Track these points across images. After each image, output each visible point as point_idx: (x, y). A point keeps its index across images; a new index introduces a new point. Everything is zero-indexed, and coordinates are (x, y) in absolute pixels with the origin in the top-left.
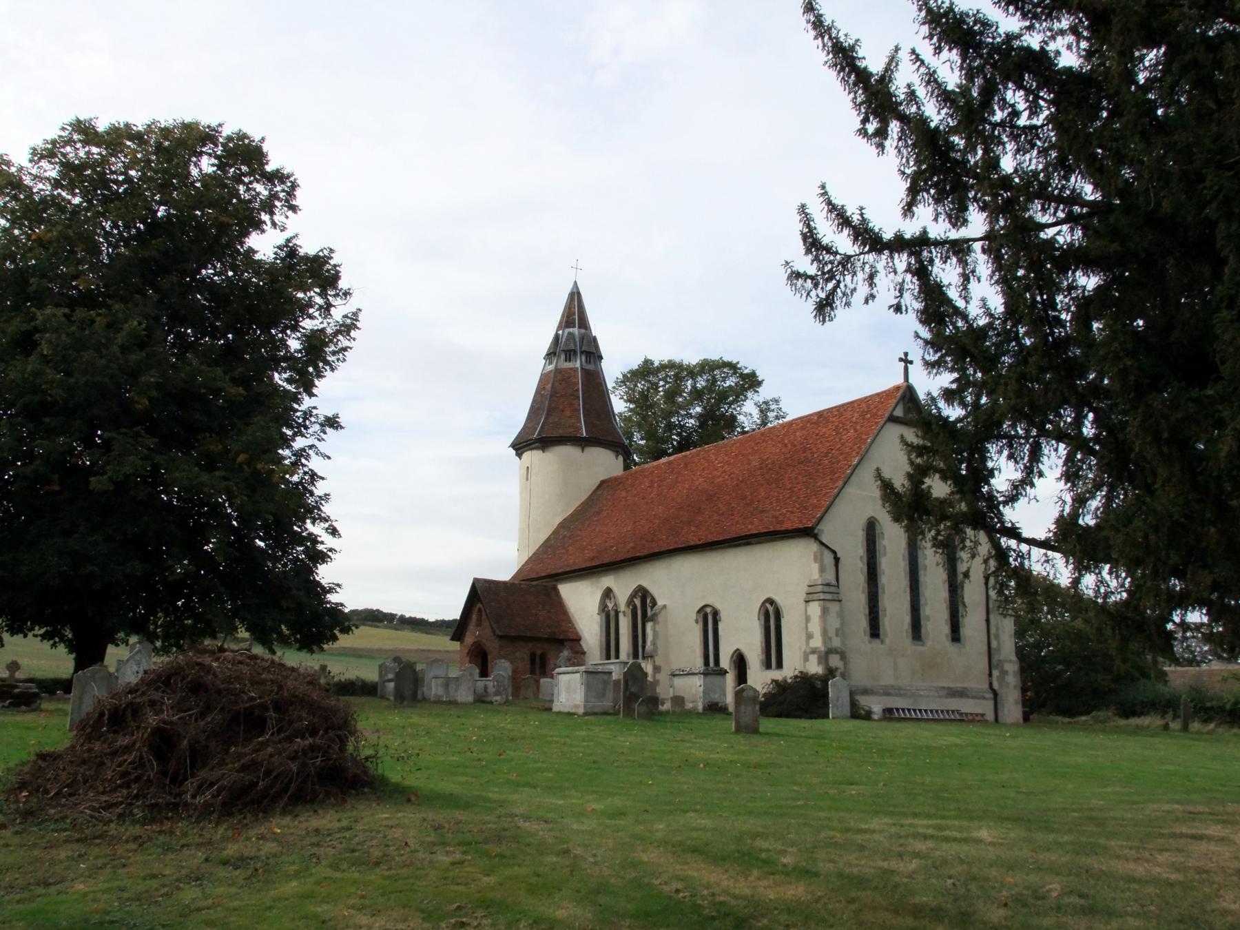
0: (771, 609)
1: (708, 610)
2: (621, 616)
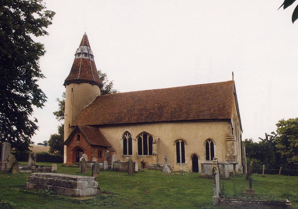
0: (210, 143)
1: (180, 141)
2: (133, 141)
